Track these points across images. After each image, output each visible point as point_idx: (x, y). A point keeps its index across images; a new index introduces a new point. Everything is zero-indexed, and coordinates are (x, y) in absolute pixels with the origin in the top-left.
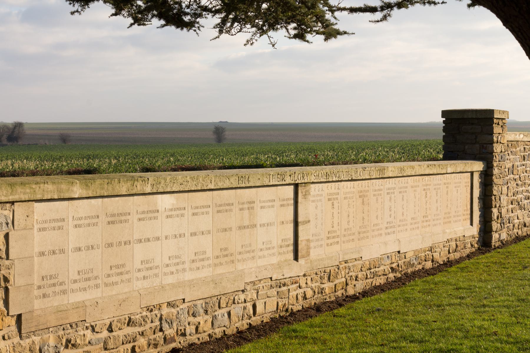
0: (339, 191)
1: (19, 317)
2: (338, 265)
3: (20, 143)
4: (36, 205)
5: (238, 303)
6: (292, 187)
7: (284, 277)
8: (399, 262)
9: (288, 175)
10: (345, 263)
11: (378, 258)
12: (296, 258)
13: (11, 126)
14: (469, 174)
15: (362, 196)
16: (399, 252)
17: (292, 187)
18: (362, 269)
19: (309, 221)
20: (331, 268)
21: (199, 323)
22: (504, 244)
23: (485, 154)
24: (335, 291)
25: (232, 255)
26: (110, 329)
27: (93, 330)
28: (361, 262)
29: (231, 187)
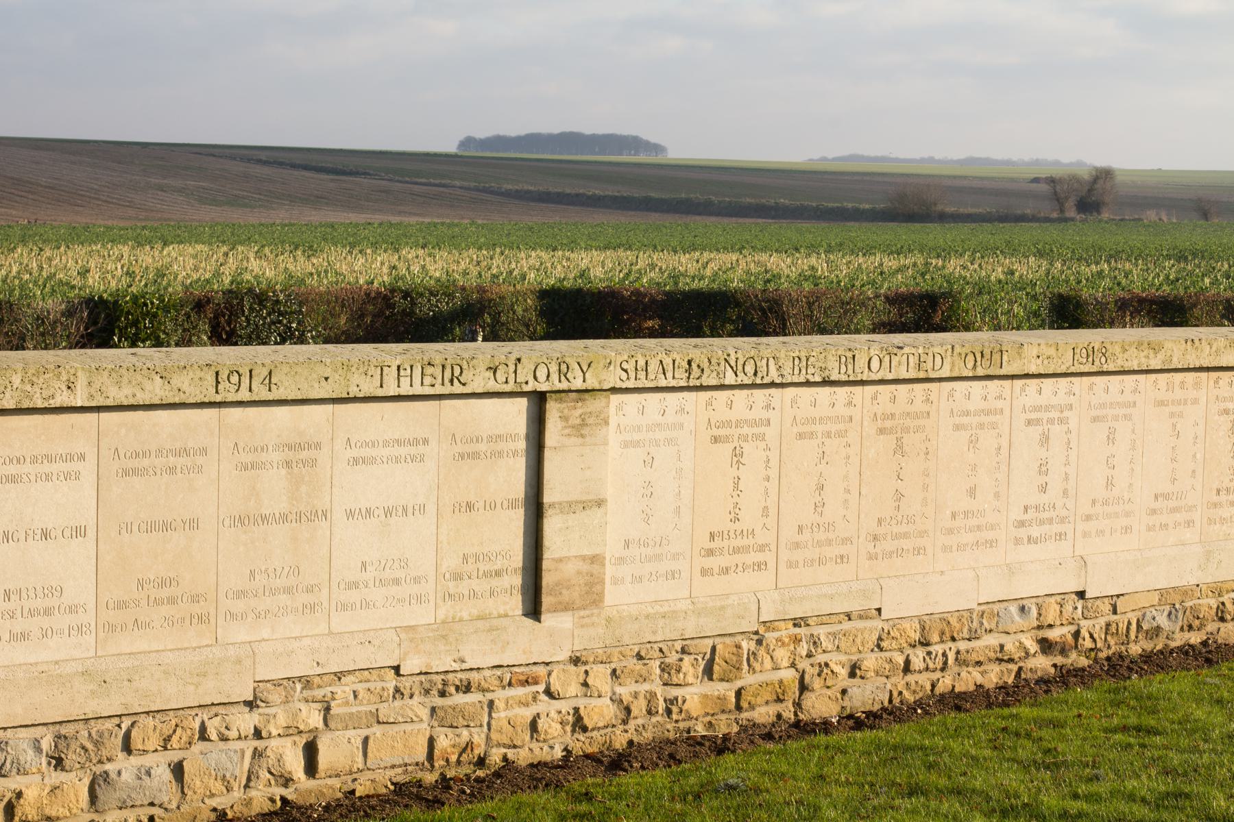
0: (770, 414)
2: (756, 633)
3: (1105, 215)
5: (224, 739)
6: (523, 402)
7: (465, 666)
8: (1083, 623)
9: (482, 367)
10: (795, 625)
11: (970, 611)
12: (534, 610)
13: (1086, 177)
16: (1081, 595)
17: (523, 402)
18: (883, 644)
19: (600, 503)
20: (718, 640)
21: (19, 795)
24: (739, 708)
25: (195, 599)
28: (877, 624)
29: (177, 400)
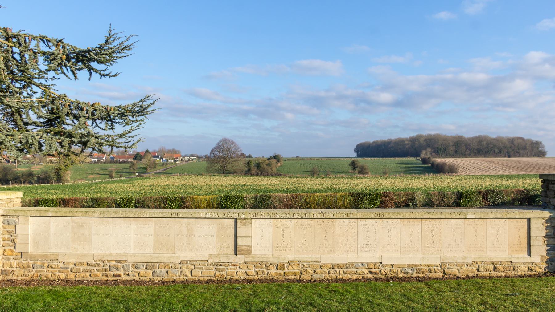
16: (381, 263)
26: (75, 265)
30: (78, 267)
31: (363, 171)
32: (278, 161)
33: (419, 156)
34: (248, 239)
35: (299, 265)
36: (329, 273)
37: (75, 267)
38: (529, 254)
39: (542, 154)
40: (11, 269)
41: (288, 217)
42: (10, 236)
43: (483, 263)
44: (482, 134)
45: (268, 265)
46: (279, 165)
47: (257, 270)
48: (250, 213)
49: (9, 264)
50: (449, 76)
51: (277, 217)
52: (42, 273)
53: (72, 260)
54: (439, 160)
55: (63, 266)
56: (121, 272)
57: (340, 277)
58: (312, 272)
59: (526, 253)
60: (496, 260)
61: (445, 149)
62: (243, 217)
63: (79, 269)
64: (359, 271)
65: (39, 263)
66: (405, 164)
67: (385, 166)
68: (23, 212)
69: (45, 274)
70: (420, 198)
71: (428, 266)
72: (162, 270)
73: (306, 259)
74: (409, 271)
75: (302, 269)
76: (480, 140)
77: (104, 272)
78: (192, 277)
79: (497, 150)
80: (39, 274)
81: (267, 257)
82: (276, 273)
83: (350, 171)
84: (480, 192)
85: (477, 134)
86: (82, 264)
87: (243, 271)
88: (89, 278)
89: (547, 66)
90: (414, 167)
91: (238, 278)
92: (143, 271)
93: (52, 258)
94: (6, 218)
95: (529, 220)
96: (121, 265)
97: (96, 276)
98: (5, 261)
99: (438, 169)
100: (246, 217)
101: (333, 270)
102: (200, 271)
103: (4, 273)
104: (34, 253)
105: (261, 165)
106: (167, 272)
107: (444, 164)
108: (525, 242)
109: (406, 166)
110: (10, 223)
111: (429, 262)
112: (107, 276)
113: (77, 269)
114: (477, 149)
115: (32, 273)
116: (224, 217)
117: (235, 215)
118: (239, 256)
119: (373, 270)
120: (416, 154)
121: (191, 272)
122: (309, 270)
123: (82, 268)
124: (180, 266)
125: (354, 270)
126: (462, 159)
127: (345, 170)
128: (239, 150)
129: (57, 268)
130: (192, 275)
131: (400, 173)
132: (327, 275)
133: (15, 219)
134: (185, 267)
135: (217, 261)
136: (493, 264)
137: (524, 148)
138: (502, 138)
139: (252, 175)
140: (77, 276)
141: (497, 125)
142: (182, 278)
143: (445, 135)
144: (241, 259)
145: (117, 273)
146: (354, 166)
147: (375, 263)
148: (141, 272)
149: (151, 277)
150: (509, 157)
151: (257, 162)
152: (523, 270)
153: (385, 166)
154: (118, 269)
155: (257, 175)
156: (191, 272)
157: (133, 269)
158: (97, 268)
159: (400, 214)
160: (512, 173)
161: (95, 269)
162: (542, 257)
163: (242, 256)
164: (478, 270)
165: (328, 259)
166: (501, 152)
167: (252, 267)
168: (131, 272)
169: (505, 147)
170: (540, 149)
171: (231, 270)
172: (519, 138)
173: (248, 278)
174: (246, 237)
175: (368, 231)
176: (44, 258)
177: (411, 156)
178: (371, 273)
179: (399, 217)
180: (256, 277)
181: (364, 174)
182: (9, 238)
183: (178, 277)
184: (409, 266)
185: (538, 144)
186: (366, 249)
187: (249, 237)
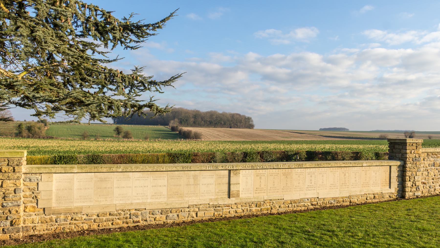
1: (44, 209)
4: (54, 174)
14: (389, 167)
15: (195, 177)
16: (318, 198)
22: (409, 199)
23: (403, 159)
26: (98, 216)
27: (87, 215)
30: (101, 218)
31: (127, 136)
32: (45, 125)
33: (167, 124)
34: (238, 185)
35: (270, 202)
36: (288, 207)
37: (98, 218)
38: (390, 188)
39: (251, 126)
40: (32, 225)
41: (265, 167)
42: (31, 193)
43: (369, 194)
44: (213, 110)
45: (250, 204)
46: (46, 128)
47: (243, 208)
48: (241, 165)
49: (31, 220)
50: (193, 64)
51: (258, 168)
52: (65, 226)
53: (96, 211)
54: (186, 129)
55: (87, 218)
56: (140, 218)
57: (295, 209)
58: (278, 207)
59: (388, 187)
60: (375, 192)
61: (187, 120)
62: (235, 169)
63: (102, 219)
64: (306, 204)
65: (62, 217)
66: (158, 131)
67: (143, 132)
68: (47, 169)
69: (68, 227)
70: (219, 156)
71: (342, 198)
72: (174, 214)
73: (275, 198)
74: (333, 202)
75: (272, 206)
76: (212, 114)
77: (125, 220)
78: (197, 218)
79: (223, 123)
80: (62, 227)
81: (250, 198)
82: (256, 209)
83: (115, 136)
84: (258, 153)
85: (209, 110)
86: (104, 214)
87: (234, 210)
88: (111, 226)
89: (259, 64)
90: (166, 134)
91: (230, 215)
92: (158, 217)
93: (76, 211)
94: (28, 176)
95: (390, 166)
96: (139, 213)
97: (118, 224)
98: (26, 218)
99: (186, 136)
100: (237, 168)
101: (291, 205)
102: (203, 212)
103: (25, 229)
104: (57, 208)
105: (33, 128)
106: (178, 215)
107: (190, 132)
108: (388, 180)
109: (160, 132)
110: (33, 180)
111: (343, 196)
112: (127, 223)
113: (100, 219)
114: (209, 121)
115: (55, 227)
116: (222, 169)
117: (230, 167)
118: (231, 199)
119: (313, 203)
120: (165, 123)
121: (197, 214)
122: (276, 205)
123: (104, 218)
124: (188, 210)
125: (303, 204)
126: (199, 128)
127: (110, 135)
128: (8, 113)
129: (81, 220)
130: (197, 216)
131: (158, 138)
132: (287, 209)
133: (38, 176)
134: (192, 210)
135: (216, 203)
136: (374, 194)
137: (241, 122)
138: (226, 113)
139: (23, 137)
140: (100, 226)
141: (223, 104)
142: (190, 219)
143: (186, 109)
144: (233, 200)
145: (136, 219)
146: (118, 131)
147: (315, 198)
148: (158, 217)
149: (165, 221)
150: (231, 128)
151: (28, 125)
152: (387, 198)
153: (143, 132)
154: (137, 217)
155: (29, 137)
156: (197, 214)
157: (150, 216)
158: (118, 217)
159: (329, 164)
160: (236, 139)
161: (117, 217)
162: (395, 188)
163: (234, 199)
164: (367, 199)
165: (288, 197)
166: (225, 124)
167: (239, 206)
168: (148, 218)
169: (228, 120)
170: (251, 123)
171: (226, 210)
172: (237, 114)
173: (236, 215)
174: (237, 184)
175: (311, 176)
176: (67, 212)
177: (161, 125)
178: (312, 205)
179: (329, 166)
180: (243, 214)
181: (128, 138)
182: (30, 195)
183: (186, 219)
184: (333, 198)
185: (249, 119)
186: (310, 189)
187: (239, 184)
